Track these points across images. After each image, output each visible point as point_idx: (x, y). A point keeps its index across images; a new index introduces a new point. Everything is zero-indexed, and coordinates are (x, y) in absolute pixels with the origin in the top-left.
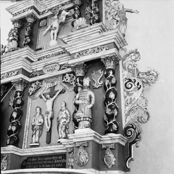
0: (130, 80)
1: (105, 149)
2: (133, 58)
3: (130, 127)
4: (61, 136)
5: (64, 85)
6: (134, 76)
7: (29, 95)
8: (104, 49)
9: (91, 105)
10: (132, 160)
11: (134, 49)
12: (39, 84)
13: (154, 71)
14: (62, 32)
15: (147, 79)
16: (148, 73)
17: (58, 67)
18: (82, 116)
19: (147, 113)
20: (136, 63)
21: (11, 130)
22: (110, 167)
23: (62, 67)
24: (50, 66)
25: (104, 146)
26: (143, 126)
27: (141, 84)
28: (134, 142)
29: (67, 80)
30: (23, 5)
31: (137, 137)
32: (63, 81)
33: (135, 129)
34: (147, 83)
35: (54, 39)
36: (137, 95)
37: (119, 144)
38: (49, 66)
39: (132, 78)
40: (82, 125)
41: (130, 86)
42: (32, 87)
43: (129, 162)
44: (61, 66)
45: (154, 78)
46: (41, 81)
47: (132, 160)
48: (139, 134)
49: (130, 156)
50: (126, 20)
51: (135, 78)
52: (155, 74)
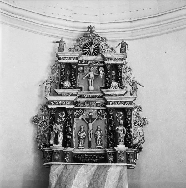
0: (137, 122)
1: (55, 153)
2: (139, 110)
3: (136, 145)
4: (98, 144)
5: (98, 116)
6: (138, 119)
7: (75, 117)
8: (127, 104)
9: (124, 135)
10: (137, 160)
11: (139, 105)
12: (81, 111)
13: (147, 118)
14: (55, 50)
15: (145, 122)
16: (144, 119)
17: (95, 104)
18: (122, 139)
19: (144, 139)
20: (139, 113)
21: (69, 138)
22: (131, 162)
23: (98, 105)
24: (90, 102)
25: (119, 152)
26: (143, 145)
27: (141, 124)
28: (139, 152)
29: (100, 113)
30: (70, 54)
31: (140, 150)
32: (98, 113)
33: (139, 146)
34: (144, 124)
35: (91, 85)
36: (139, 129)
37: (62, 151)
38: (89, 102)
39: (138, 121)
40: (121, 143)
41: (136, 124)
42: (76, 112)
43: (136, 160)
44: (97, 104)
45: (147, 122)
46: (83, 110)
47: (137, 160)
48: (141, 149)
49: (137, 158)
50: (137, 88)
51: (139, 121)
52: (147, 120)
